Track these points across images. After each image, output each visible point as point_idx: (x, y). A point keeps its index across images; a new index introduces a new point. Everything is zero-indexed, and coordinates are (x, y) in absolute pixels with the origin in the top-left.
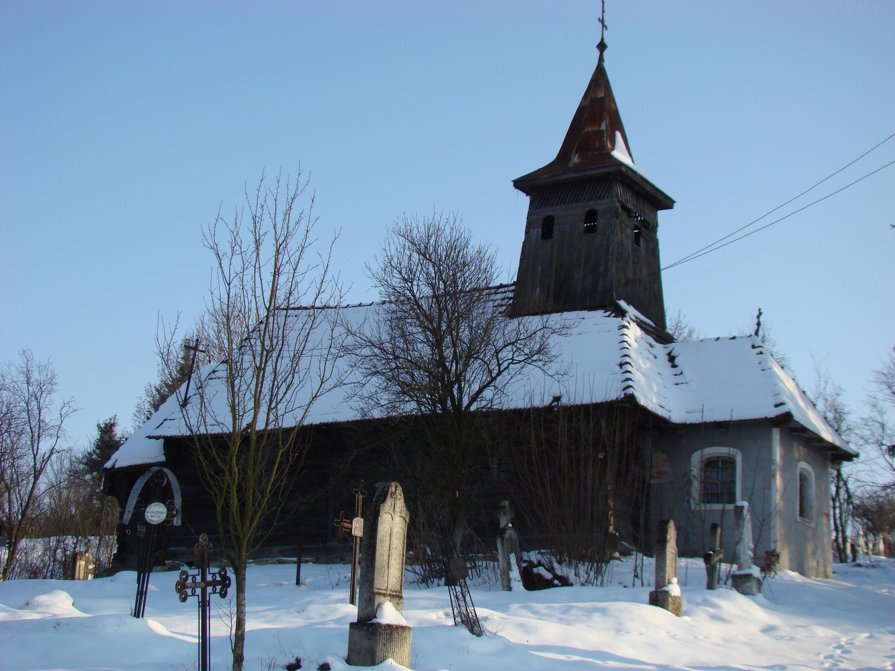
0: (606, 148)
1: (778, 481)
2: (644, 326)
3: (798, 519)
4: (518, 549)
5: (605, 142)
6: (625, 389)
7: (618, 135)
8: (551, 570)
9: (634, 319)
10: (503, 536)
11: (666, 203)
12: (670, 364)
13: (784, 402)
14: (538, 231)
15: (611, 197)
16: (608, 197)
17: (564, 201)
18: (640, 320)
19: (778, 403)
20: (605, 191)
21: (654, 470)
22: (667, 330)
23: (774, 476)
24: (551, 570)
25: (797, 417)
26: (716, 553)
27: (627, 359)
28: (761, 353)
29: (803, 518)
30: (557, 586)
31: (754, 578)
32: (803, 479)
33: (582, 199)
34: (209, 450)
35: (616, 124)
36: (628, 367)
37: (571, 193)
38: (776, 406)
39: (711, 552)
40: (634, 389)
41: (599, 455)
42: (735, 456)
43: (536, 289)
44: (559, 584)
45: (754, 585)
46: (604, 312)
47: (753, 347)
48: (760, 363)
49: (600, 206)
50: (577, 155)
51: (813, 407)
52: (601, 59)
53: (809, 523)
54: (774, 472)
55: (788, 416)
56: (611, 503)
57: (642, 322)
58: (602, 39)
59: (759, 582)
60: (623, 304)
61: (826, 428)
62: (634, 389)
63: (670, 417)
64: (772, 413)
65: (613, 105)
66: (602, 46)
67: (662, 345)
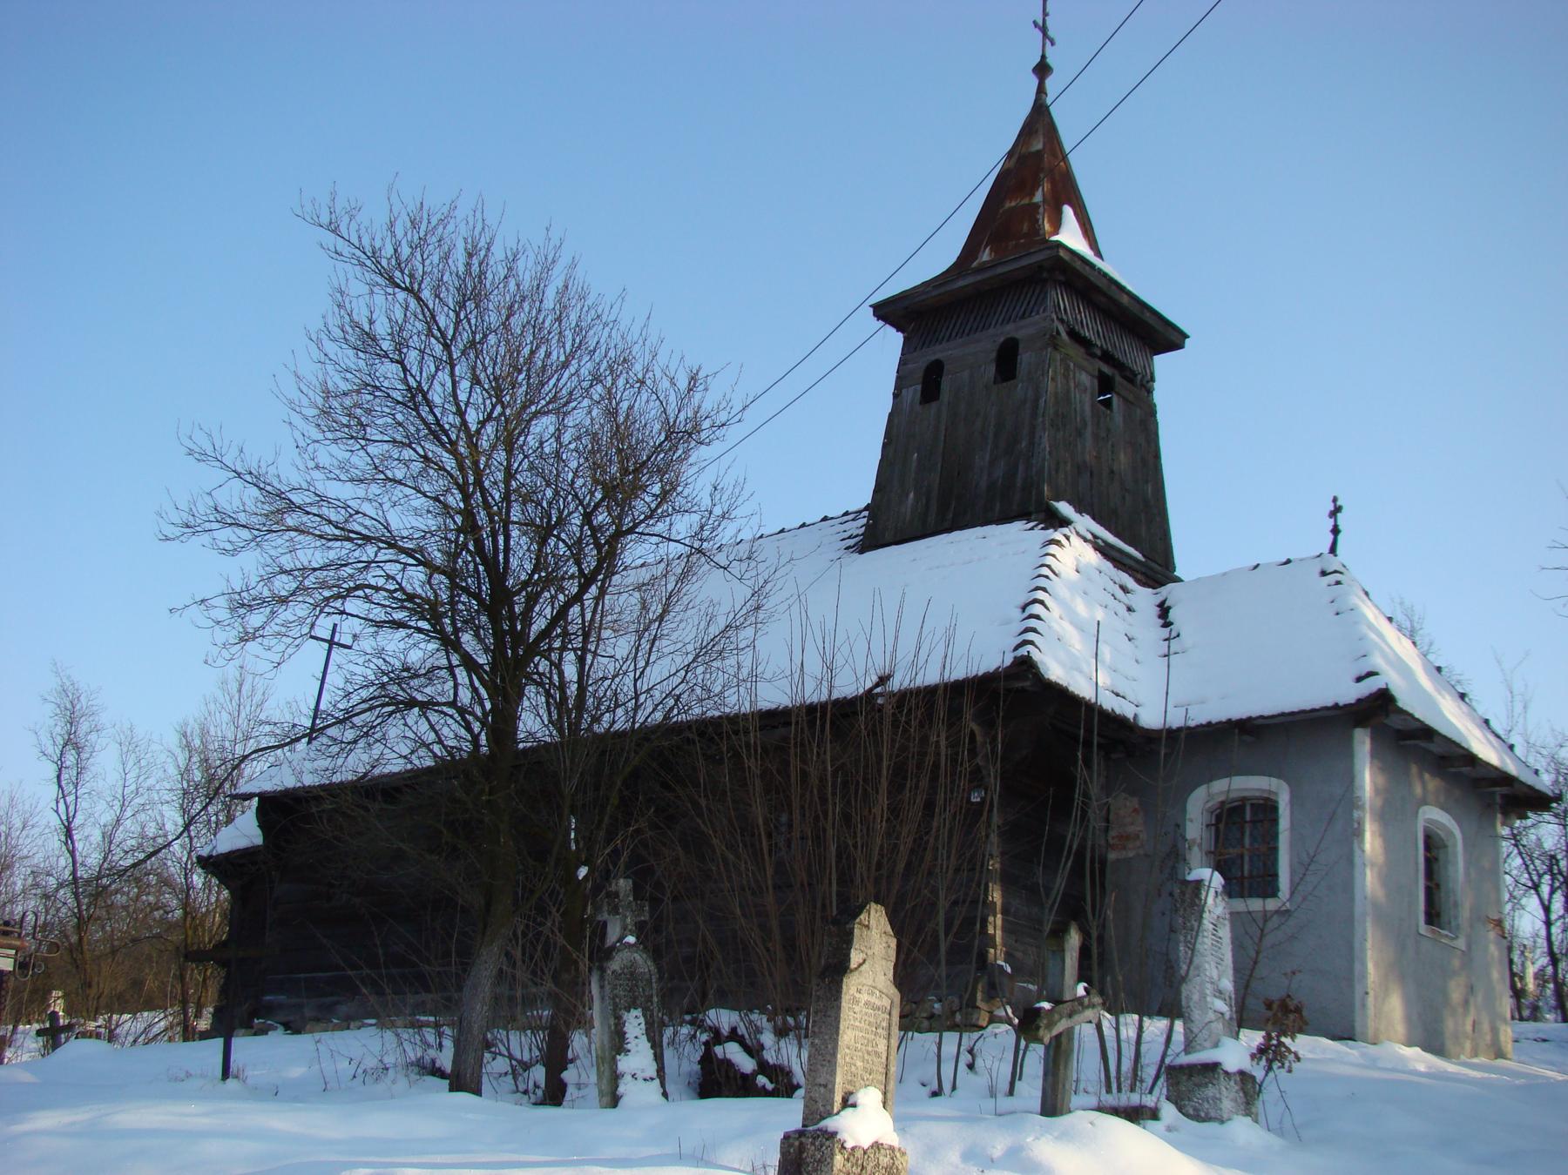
0: (1041, 232)
1: (1371, 841)
2: (1114, 554)
3: (1423, 928)
4: (655, 999)
5: (1040, 221)
6: (1016, 649)
7: (1068, 212)
9: (1089, 537)
10: (605, 965)
11: (1166, 337)
12: (1161, 622)
14: (915, 390)
16: (1038, 313)
18: (1103, 541)
19: (1363, 673)
21: (1112, 833)
23: (1358, 833)
24: (754, 1050)
25: (1405, 701)
26: (1065, 1008)
27: (1040, 595)
28: (1338, 583)
30: (763, 1093)
31: (1226, 1073)
32: (1433, 845)
33: (993, 323)
34: (1047, 911)
35: (1066, 192)
36: (1037, 609)
38: (1359, 679)
39: (1046, 1005)
42: (1276, 794)
43: (907, 495)
44: (770, 1086)
45: (1227, 1093)
47: (1324, 573)
49: (1021, 330)
51: (1459, 700)
52: (1041, 90)
54: (1359, 823)
55: (1383, 701)
56: (996, 896)
57: (1112, 547)
58: (1043, 57)
59: (1248, 1086)
60: (1064, 508)
61: (1484, 735)
63: (1136, 716)
64: (1349, 693)
65: (1062, 164)
66: (1042, 70)
67: (1150, 590)
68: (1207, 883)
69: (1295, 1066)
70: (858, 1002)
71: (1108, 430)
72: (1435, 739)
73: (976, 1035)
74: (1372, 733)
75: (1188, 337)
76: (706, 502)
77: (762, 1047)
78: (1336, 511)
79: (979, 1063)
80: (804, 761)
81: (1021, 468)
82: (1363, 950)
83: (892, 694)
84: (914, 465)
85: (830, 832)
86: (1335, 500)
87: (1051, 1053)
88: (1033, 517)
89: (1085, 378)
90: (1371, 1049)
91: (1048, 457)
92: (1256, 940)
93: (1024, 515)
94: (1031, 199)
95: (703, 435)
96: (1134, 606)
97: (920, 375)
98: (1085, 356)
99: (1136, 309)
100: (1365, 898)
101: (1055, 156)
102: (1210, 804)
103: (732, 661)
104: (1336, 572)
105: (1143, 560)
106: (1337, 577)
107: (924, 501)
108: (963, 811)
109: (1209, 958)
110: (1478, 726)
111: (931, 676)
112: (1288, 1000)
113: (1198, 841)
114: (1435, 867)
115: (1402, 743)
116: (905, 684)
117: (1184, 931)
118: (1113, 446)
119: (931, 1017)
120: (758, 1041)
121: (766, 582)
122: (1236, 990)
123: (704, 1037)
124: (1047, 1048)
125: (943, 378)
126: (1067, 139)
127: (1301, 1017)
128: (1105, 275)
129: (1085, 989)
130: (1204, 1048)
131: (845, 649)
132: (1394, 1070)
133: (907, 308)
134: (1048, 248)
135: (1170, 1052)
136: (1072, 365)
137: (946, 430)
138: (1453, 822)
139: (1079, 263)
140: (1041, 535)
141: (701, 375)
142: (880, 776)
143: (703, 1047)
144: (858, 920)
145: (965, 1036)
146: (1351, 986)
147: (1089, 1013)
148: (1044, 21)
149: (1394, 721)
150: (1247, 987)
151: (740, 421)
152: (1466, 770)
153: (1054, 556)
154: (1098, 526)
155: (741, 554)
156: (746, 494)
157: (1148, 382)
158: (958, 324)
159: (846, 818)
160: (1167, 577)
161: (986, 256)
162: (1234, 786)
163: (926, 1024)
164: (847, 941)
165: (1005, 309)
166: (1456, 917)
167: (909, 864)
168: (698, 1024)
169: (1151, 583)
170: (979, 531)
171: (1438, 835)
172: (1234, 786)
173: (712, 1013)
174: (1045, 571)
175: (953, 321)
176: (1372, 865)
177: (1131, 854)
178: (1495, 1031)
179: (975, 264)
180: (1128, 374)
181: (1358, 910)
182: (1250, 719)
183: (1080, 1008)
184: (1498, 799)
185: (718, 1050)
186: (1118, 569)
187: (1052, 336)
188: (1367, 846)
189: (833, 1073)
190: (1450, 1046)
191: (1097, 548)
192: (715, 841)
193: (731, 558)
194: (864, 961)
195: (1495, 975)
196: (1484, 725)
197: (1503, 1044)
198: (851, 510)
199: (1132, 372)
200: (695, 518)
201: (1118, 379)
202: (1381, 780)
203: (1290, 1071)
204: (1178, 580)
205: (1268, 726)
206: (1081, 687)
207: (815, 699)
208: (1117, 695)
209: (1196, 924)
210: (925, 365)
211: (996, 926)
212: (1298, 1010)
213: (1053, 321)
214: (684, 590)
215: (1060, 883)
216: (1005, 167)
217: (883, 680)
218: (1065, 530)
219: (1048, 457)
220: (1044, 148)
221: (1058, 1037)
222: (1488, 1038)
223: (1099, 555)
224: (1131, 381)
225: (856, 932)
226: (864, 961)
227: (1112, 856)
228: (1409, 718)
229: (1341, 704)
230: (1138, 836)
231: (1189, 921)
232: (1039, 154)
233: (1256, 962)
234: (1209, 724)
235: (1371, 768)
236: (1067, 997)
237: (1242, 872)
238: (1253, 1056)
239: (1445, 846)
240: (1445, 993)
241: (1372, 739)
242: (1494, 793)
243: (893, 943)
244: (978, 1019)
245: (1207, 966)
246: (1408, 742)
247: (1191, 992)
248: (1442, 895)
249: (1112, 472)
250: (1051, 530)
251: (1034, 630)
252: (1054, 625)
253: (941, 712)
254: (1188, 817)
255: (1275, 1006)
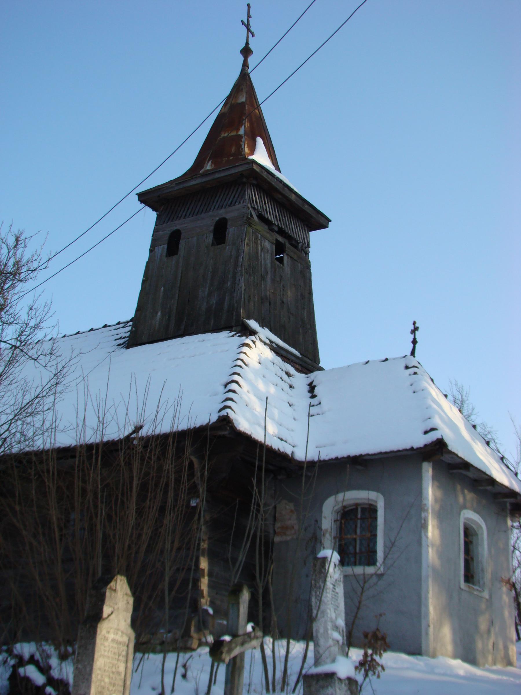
3: (463, 585)
5: (243, 147)
6: (220, 411)
7: (260, 141)
8: (45, 670)
9: (268, 342)
13: (435, 427)
14: (163, 248)
15: (243, 202)
17: (192, 212)
18: (276, 345)
19: (428, 429)
20: (237, 196)
21: (278, 525)
22: (320, 365)
23: (425, 526)
24: (45, 670)
25: (453, 446)
26: (239, 640)
27: (236, 378)
28: (415, 373)
29: (471, 585)
31: (340, 679)
33: (212, 209)
36: (234, 386)
37: (200, 203)
38: (426, 433)
39: (227, 638)
40: (233, 410)
41: (191, 502)
42: (376, 502)
43: (157, 313)
46: (230, 333)
47: (407, 367)
48: (411, 385)
50: (210, 163)
52: (245, 65)
53: (480, 591)
54: (425, 520)
56: (204, 564)
58: (247, 44)
60: (253, 324)
62: (233, 410)
63: (293, 453)
65: (257, 111)
66: (246, 51)
67: (304, 375)
68: (329, 559)
69: (382, 674)
70: (107, 640)
71: (281, 277)
72: (471, 469)
73: (188, 655)
74: (433, 464)
75: (331, 221)
76: (24, 316)
77: (50, 667)
78: (415, 330)
79: (189, 674)
80: (84, 481)
81: (227, 299)
82: (427, 598)
83: (142, 438)
84: (161, 294)
85: (99, 527)
86: (414, 323)
87: (230, 668)
88: (233, 329)
89: (267, 245)
90: (432, 661)
91: (243, 292)
92: (359, 594)
93: (228, 328)
94: (237, 132)
95: (23, 275)
96: (294, 385)
97: (167, 238)
98: (268, 231)
99: (299, 203)
100: (428, 566)
101: (252, 105)
102: (336, 508)
103: (39, 417)
104: (414, 367)
105: (300, 356)
106: (415, 370)
107: (167, 318)
108: (183, 513)
109: (330, 606)
110: (497, 462)
111: (165, 428)
112: (377, 633)
113: (329, 530)
114: (471, 547)
115: (451, 471)
116: (149, 433)
117: (315, 589)
118: (283, 287)
119: (162, 643)
120: (48, 663)
121: (64, 367)
122: (347, 625)
123: (12, 662)
124: (228, 666)
125: (181, 241)
126: (261, 95)
127: (385, 643)
128: (281, 181)
129: (253, 627)
130: (326, 663)
131: (112, 411)
132: (444, 674)
133: (159, 196)
134: (248, 163)
135: (306, 665)
136: (260, 235)
137: (182, 273)
138: (481, 519)
139: (266, 173)
140: (238, 340)
141: (22, 237)
142: (131, 491)
143: (11, 669)
144: (109, 587)
145: (181, 655)
146: (420, 622)
147: (255, 643)
148: (248, 21)
149: (446, 458)
150: (353, 623)
151: (46, 268)
152: (489, 488)
153: (245, 353)
154: (273, 335)
155: (46, 351)
156: (51, 311)
157: (306, 248)
158: (191, 208)
159: (109, 517)
160: (314, 367)
161: (209, 166)
162: (346, 498)
163: (159, 647)
164: (101, 600)
165: (220, 199)
166: (483, 578)
167: (149, 545)
168: (10, 652)
169: (304, 370)
170: (200, 337)
171: (472, 527)
172: (346, 498)
173: (18, 646)
174: (240, 363)
175: (187, 207)
176: (433, 545)
177: (289, 538)
178: (506, 648)
179: (202, 171)
180: (294, 242)
181: (424, 573)
182: (361, 456)
183: (249, 639)
184: (508, 506)
185: (21, 671)
186: (285, 361)
187: (248, 218)
188: (430, 534)
189: (89, 687)
190: (480, 658)
191: (272, 349)
192: (24, 533)
193: (39, 353)
194: (112, 613)
195: (506, 613)
196: (501, 461)
197: (511, 657)
198: (122, 321)
199: (297, 241)
200: (18, 327)
201: (287, 245)
202: (439, 494)
203: (378, 676)
204: (321, 369)
205: (372, 460)
206: (258, 435)
207: (92, 441)
208: (282, 440)
209: (322, 585)
210: (169, 233)
211: (204, 584)
212: (383, 638)
213: (248, 208)
214: (11, 371)
215: (242, 557)
216: (223, 111)
217: (138, 429)
218: (253, 338)
219: (243, 292)
220: (246, 101)
221: (235, 658)
222: (502, 653)
223: (273, 353)
224: (296, 247)
225: (108, 594)
226: (112, 613)
227: (277, 539)
228: (454, 456)
229: (415, 447)
230: (293, 527)
231: (318, 583)
232: (243, 104)
233: (358, 608)
234: (337, 458)
235: (432, 486)
236: (241, 632)
237: (355, 550)
238: (356, 668)
239: (476, 534)
240: (477, 627)
241: (434, 469)
242: (505, 502)
243: (131, 600)
244: (192, 644)
245: (329, 611)
246: (455, 471)
247: (318, 627)
248: (475, 564)
249: (283, 302)
250: (244, 338)
251: (231, 400)
252: (244, 396)
253: (171, 452)
254: (323, 515)
255: (370, 636)
